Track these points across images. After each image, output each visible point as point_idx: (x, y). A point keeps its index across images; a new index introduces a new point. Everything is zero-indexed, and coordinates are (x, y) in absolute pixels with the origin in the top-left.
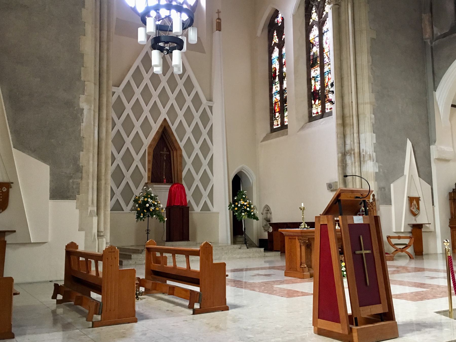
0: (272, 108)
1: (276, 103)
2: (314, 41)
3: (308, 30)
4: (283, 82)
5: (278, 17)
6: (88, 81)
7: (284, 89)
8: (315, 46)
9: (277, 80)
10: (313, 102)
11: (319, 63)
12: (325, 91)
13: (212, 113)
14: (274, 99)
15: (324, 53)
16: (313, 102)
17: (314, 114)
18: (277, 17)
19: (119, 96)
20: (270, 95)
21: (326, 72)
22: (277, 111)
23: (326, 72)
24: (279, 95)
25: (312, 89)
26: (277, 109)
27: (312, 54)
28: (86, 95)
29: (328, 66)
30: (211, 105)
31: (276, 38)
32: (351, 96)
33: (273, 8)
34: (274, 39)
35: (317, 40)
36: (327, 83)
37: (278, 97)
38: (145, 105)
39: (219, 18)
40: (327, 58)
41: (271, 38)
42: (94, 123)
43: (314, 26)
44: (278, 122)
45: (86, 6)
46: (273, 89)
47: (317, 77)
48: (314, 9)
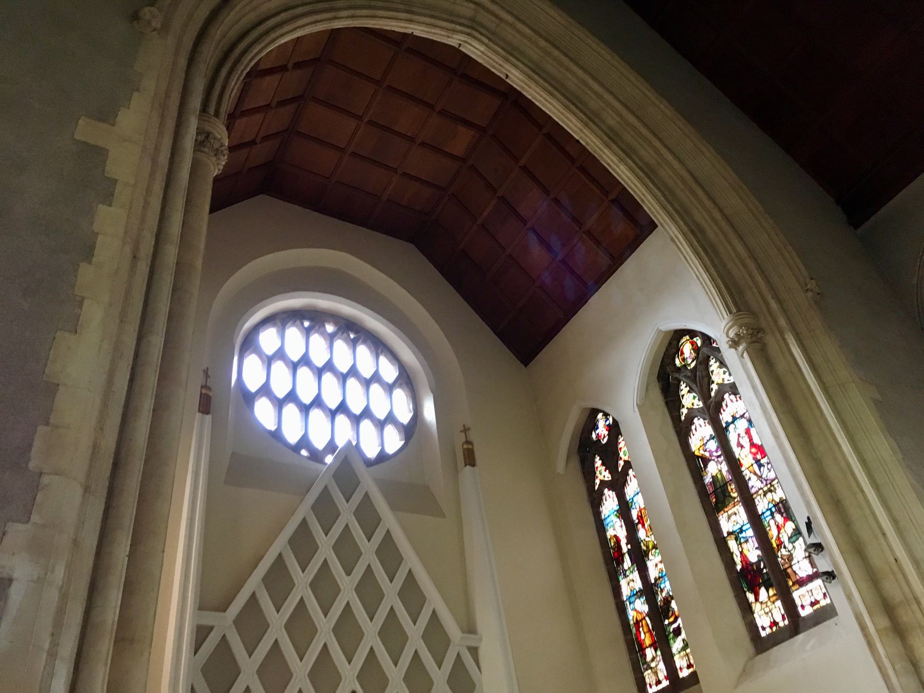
0: (629, 637)
1: (637, 623)
2: (705, 451)
3: (683, 430)
4: (646, 565)
5: (598, 428)
6: (56, 474)
7: (653, 581)
8: (710, 460)
9: (627, 563)
10: (751, 597)
11: (735, 495)
12: (779, 559)
13: (479, 667)
14: (632, 615)
15: (743, 469)
16: (751, 597)
17: (764, 629)
18: (595, 427)
19: (224, 636)
20: (617, 604)
21: (763, 513)
22: (648, 642)
23: (763, 513)
24: (643, 599)
25: (735, 564)
26: (646, 639)
27: (708, 480)
28: (35, 523)
29: (765, 495)
30: (473, 644)
31: (603, 470)
32: (884, 543)
33: (586, 409)
34: (598, 473)
35: (713, 445)
36: (778, 538)
37: (641, 606)
38: (296, 656)
39: (469, 440)
40: (754, 478)
41: (590, 473)
42: (55, 644)
43: (695, 420)
44: (656, 673)
45: (94, 260)
46: (621, 588)
47: (741, 531)
48: (683, 386)
